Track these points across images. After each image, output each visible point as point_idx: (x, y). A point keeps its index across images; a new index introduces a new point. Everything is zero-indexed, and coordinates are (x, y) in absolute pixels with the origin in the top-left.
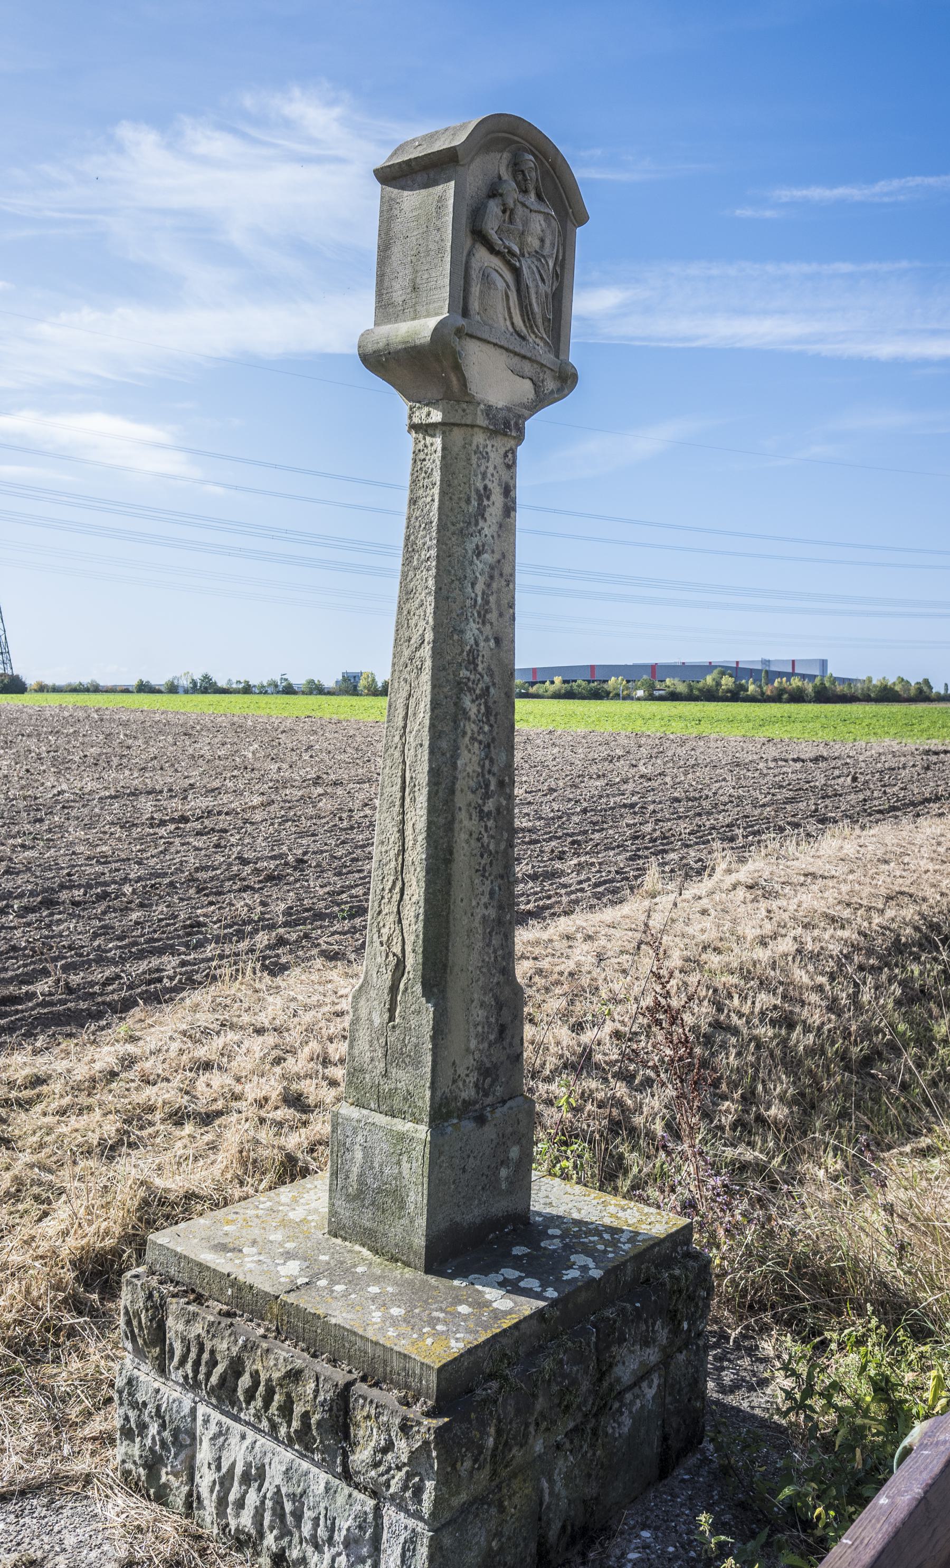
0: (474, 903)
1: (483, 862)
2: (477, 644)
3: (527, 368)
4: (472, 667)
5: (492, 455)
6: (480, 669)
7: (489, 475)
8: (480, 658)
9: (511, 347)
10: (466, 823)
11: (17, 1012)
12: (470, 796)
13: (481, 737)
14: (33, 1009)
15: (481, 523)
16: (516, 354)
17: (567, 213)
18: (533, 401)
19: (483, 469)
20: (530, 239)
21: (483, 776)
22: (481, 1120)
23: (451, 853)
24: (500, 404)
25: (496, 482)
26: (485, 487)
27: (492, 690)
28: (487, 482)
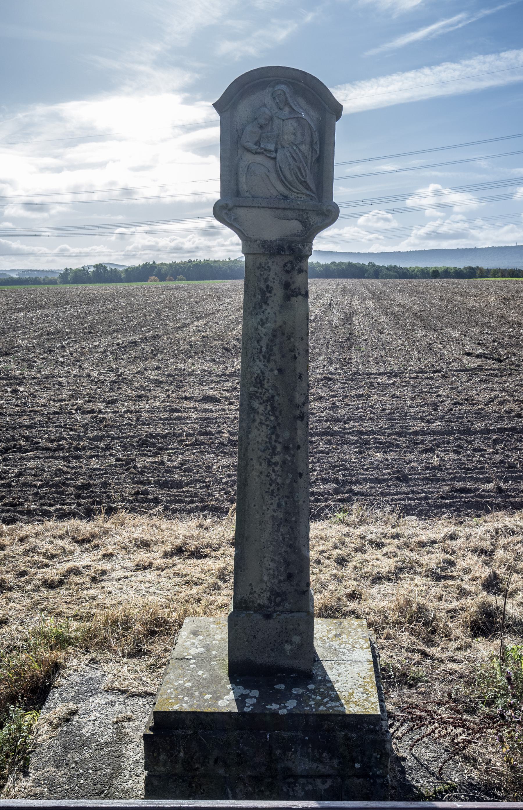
0: (264, 508)
1: (271, 488)
2: (263, 373)
3: (290, 214)
4: (259, 385)
6: (266, 386)
7: (271, 279)
8: (266, 381)
10: (257, 467)
11: (462, 497)
12: (260, 453)
13: (268, 423)
14: (472, 497)
15: (264, 307)
16: (277, 209)
18: (302, 231)
19: (265, 276)
20: (286, 137)
21: (270, 443)
22: (268, 617)
23: (246, 481)
24: (274, 238)
26: (268, 287)
27: (276, 398)
28: (269, 283)
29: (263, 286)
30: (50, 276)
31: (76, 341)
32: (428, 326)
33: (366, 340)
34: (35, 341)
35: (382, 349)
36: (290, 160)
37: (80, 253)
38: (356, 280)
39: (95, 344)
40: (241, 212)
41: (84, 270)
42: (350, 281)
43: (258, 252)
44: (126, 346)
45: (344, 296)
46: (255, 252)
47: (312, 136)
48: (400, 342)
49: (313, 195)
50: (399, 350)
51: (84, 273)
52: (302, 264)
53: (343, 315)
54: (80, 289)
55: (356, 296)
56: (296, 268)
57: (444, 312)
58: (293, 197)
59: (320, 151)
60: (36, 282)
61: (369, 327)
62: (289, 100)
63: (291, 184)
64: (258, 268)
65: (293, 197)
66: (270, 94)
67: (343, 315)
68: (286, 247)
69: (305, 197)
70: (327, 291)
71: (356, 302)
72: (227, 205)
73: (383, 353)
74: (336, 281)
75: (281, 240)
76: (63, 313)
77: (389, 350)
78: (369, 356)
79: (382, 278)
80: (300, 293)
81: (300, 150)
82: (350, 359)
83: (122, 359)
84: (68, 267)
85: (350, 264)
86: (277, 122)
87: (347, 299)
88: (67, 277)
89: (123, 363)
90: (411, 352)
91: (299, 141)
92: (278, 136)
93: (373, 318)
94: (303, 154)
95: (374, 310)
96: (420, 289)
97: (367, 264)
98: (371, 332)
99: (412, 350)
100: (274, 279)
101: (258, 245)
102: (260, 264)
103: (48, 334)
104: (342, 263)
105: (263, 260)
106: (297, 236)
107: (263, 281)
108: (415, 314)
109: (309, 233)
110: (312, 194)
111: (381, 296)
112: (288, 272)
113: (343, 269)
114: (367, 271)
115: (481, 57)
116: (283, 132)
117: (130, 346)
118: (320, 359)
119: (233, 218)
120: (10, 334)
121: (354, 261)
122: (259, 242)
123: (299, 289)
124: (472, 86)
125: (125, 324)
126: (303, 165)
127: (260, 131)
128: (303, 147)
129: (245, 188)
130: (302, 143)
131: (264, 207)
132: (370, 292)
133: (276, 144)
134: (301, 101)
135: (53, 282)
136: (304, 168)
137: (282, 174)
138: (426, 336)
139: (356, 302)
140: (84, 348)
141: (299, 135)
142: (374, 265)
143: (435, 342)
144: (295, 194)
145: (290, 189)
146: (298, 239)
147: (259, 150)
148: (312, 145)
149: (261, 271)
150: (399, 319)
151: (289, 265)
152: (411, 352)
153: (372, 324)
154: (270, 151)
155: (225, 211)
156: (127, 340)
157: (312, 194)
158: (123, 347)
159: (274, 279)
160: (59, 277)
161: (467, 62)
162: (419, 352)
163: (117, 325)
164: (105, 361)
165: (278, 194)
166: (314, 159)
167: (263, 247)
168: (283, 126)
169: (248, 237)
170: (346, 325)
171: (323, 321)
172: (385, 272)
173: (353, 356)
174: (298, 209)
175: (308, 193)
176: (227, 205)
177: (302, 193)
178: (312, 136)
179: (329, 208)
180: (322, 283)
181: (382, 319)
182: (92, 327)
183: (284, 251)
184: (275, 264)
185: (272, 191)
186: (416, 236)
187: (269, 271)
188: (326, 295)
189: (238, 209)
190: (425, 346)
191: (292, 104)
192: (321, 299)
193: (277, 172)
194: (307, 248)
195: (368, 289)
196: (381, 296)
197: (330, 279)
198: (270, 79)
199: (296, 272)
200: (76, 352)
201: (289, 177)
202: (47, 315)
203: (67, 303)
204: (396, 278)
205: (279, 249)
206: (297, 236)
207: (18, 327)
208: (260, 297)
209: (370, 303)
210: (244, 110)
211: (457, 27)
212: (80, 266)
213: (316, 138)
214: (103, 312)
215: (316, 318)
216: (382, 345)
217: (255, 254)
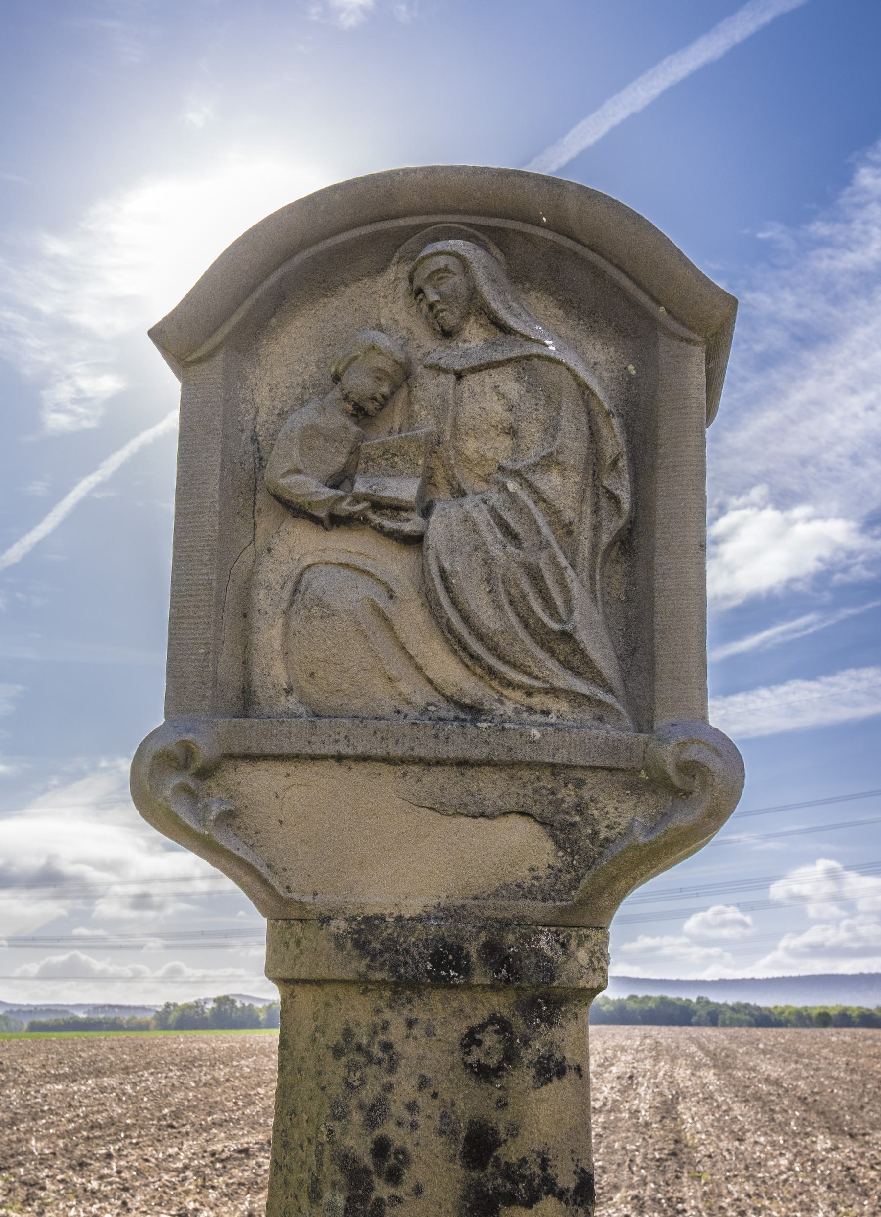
3: (491, 787)
5: (408, 1050)
7: (397, 1109)
9: (397, 751)
16: (428, 763)
17: (652, 320)
18: (556, 873)
19: (368, 1095)
20: (470, 446)
24: (413, 908)
25: (428, 1124)
26: (381, 1148)
28: (388, 1129)
29: (358, 1144)
30: (140, 1017)
31: (137, 1143)
32: (834, 1127)
33: (710, 1156)
34: (61, 1143)
35: (748, 1179)
36: (491, 536)
37: (204, 977)
38: (677, 1029)
39: (171, 1151)
40: (259, 783)
41: (197, 1007)
42: (665, 1029)
43: (336, 973)
44: (227, 1159)
45: (656, 1060)
46: (322, 972)
47: (594, 435)
48: (784, 1162)
49: (608, 699)
50: (785, 1181)
51: (197, 1012)
52: (556, 1033)
53: (659, 1099)
54: (181, 1040)
55: (681, 1061)
56: (528, 1055)
57: (862, 1096)
58: (509, 708)
59: (635, 504)
60: (114, 1026)
61: (712, 1126)
62: (487, 290)
63: (494, 649)
64: (338, 1052)
65: (509, 708)
66: (404, 286)
67: (659, 1099)
68: (473, 949)
69: (564, 706)
70: (623, 1050)
71: (681, 1071)
72: (188, 752)
73: (749, 1187)
74: (638, 1031)
75: (451, 913)
76: (134, 1084)
77: (764, 1182)
78: (720, 1196)
79: (724, 1025)
80: (549, 1186)
81: (539, 497)
82: (682, 1200)
83: (213, 1187)
84: (172, 1001)
85: (663, 1000)
86: (430, 388)
87: (664, 1067)
88: (167, 1019)
89: (213, 1195)
90: (812, 1188)
91: (531, 457)
92: (433, 445)
93: (718, 1107)
94: (554, 513)
95: (721, 1091)
96: (802, 1048)
97: (694, 1000)
98: (718, 1137)
99: (813, 1183)
100: (412, 1107)
101: (339, 941)
102: (348, 1034)
103: (92, 1128)
104: (648, 998)
105: (359, 1011)
106: (530, 894)
107: (357, 1117)
108: (803, 1100)
109: (590, 882)
110: (601, 695)
111: (730, 1060)
112: (484, 1073)
113: (651, 1009)
114: (694, 1013)
115: (852, 672)
116: (455, 427)
117: (236, 1159)
118: (617, 1197)
119: (215, 810)
120: (23, 1126)
121: (671, 995)
122: (339, 925)
123: (544, 1163)
124: (845, 713)
125: (239, 1109)
126: (553, 559)
127: (355, 429)
128: (552, 483)
129: (279, 674)
130: (548, 462)
131: (364, 758)
132: (707, 1053)
133: (428, 481)
134: (539, 302)
135: (143, 1027)
136: (560, 572)
137: (454, 602)
138: (835, 1148)
139: (682, 1073)
140: (147, 1160)
141: (532, 432)
142: (708, 1003)
143: (859, 1164)
144: (518, 695)
145: (491, 672)
146: (535, 909)
147: (345, 508)
148: (596, 476)
149: (352, 1067)
150: (772, 1111)
151: (490, 1039)
152: (812, 1188)
153: (718, 1120)
154: (396, 508)
155: (175, 780)
156: (233, 1146)
157: (601, 695)
158: (222, 1161)
159: (412, 1107)
160: (155, 1018)
161: (830, 679)
162: (829, 1187)
163: (223, 1111)
164: (180, 1189)
165: (435, 697)
166: (605, 538)
167: (361, 946)
168: (458, 400)
169: (289, 902)
170: (667, 1121)
171: (620, 1112)
172: (729, 1014)
173: (688, 1192)
174: (531, 765)
175: (581, 687)
176: (188, 752)
177: (552, 691)
178: (594, 435)
179: (692, 753)
180: (613, 1035)
181: (738, 1109)
182: (176, 1115)
183: (466, 971)
184: (417, 1031)
185: (404, 688)
186: (786, 949)
187: (391, 1070)
188: (623, 1058)
189: (245, 768)
190: (839, 1174)
191: (496, 306)
192: (612, 1065)
193: (433, 607)
194: (582, 956)
195: (701, 1047)
196: (730, 1060)
197: (627, 1027)
198: (402, 222)
199: (528, 1075)
200: (129, 1168)
201: (486, 615)
202: (103, 1090)
203: (148, 1066)
204: (750, 1025)
205: (438, 959)
206: (530, 894)
207: (42, 1111)
208: (340, 1201)
209: (710, 1076)
210: (290, 358)
211: (805, 633)
212: (191, 1000)
213: (614, 440)
214: (205, 1085)
215: (605, 1104)
216: (747, 1168)
217: (319, 983)
